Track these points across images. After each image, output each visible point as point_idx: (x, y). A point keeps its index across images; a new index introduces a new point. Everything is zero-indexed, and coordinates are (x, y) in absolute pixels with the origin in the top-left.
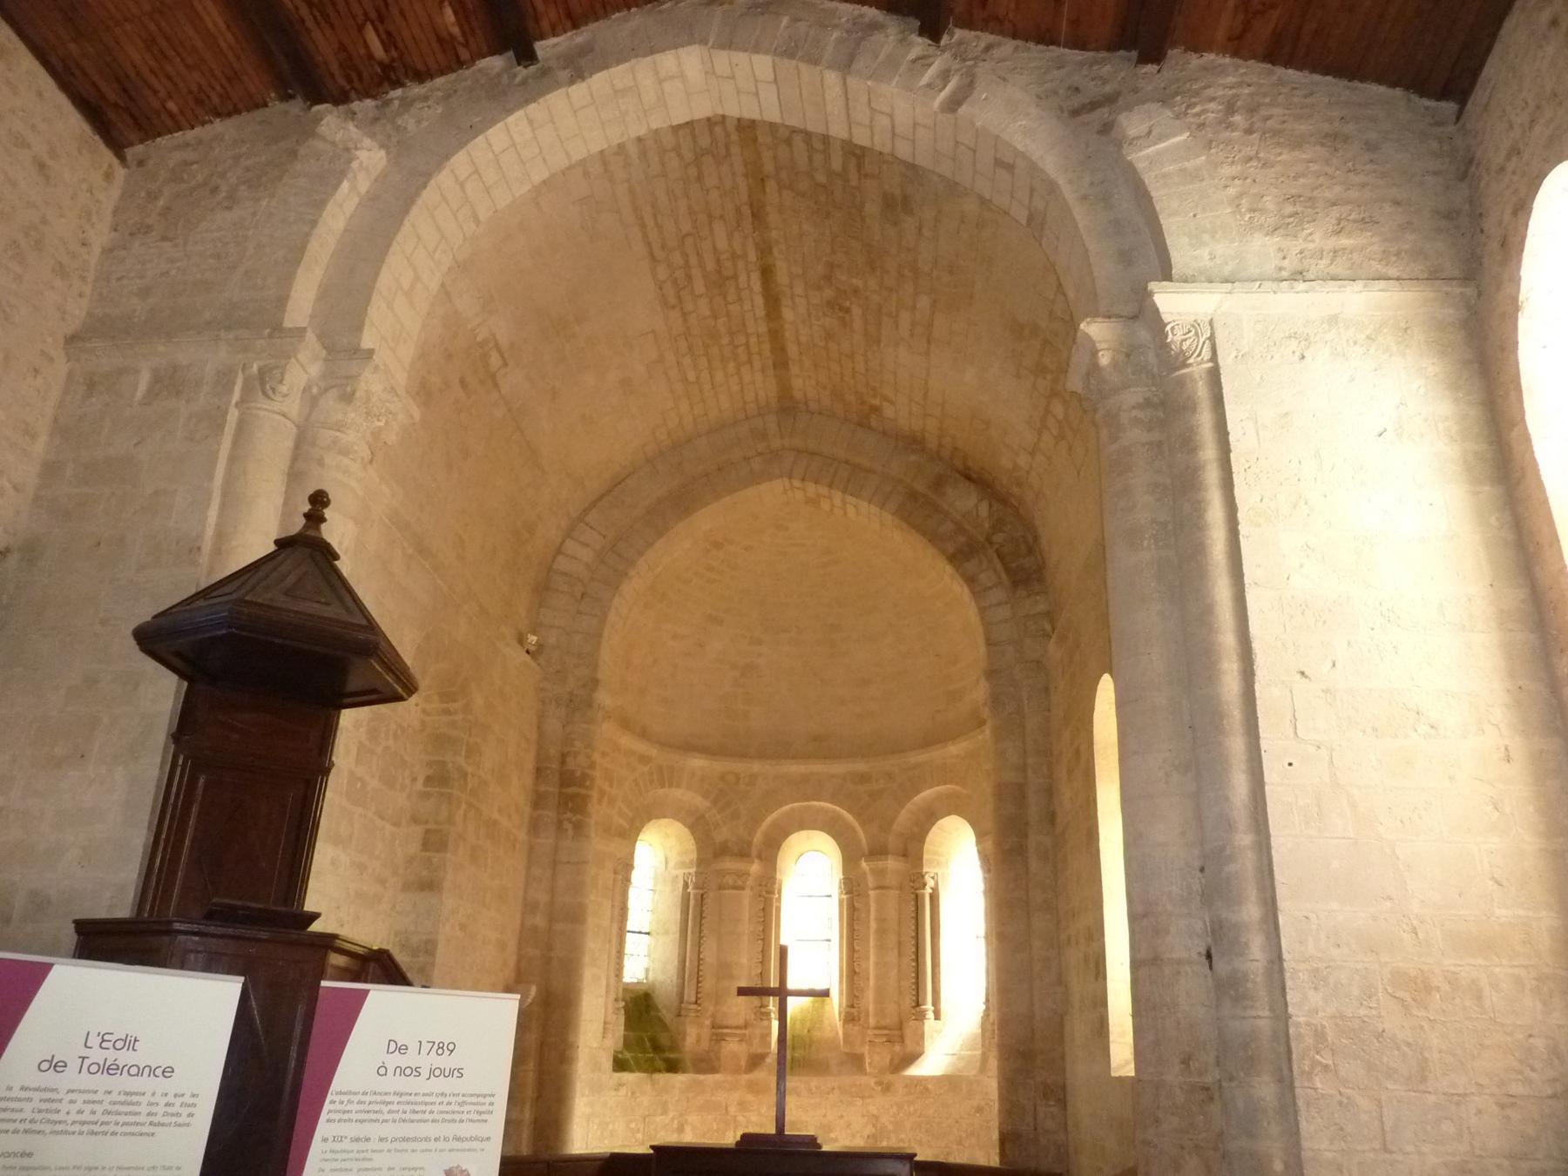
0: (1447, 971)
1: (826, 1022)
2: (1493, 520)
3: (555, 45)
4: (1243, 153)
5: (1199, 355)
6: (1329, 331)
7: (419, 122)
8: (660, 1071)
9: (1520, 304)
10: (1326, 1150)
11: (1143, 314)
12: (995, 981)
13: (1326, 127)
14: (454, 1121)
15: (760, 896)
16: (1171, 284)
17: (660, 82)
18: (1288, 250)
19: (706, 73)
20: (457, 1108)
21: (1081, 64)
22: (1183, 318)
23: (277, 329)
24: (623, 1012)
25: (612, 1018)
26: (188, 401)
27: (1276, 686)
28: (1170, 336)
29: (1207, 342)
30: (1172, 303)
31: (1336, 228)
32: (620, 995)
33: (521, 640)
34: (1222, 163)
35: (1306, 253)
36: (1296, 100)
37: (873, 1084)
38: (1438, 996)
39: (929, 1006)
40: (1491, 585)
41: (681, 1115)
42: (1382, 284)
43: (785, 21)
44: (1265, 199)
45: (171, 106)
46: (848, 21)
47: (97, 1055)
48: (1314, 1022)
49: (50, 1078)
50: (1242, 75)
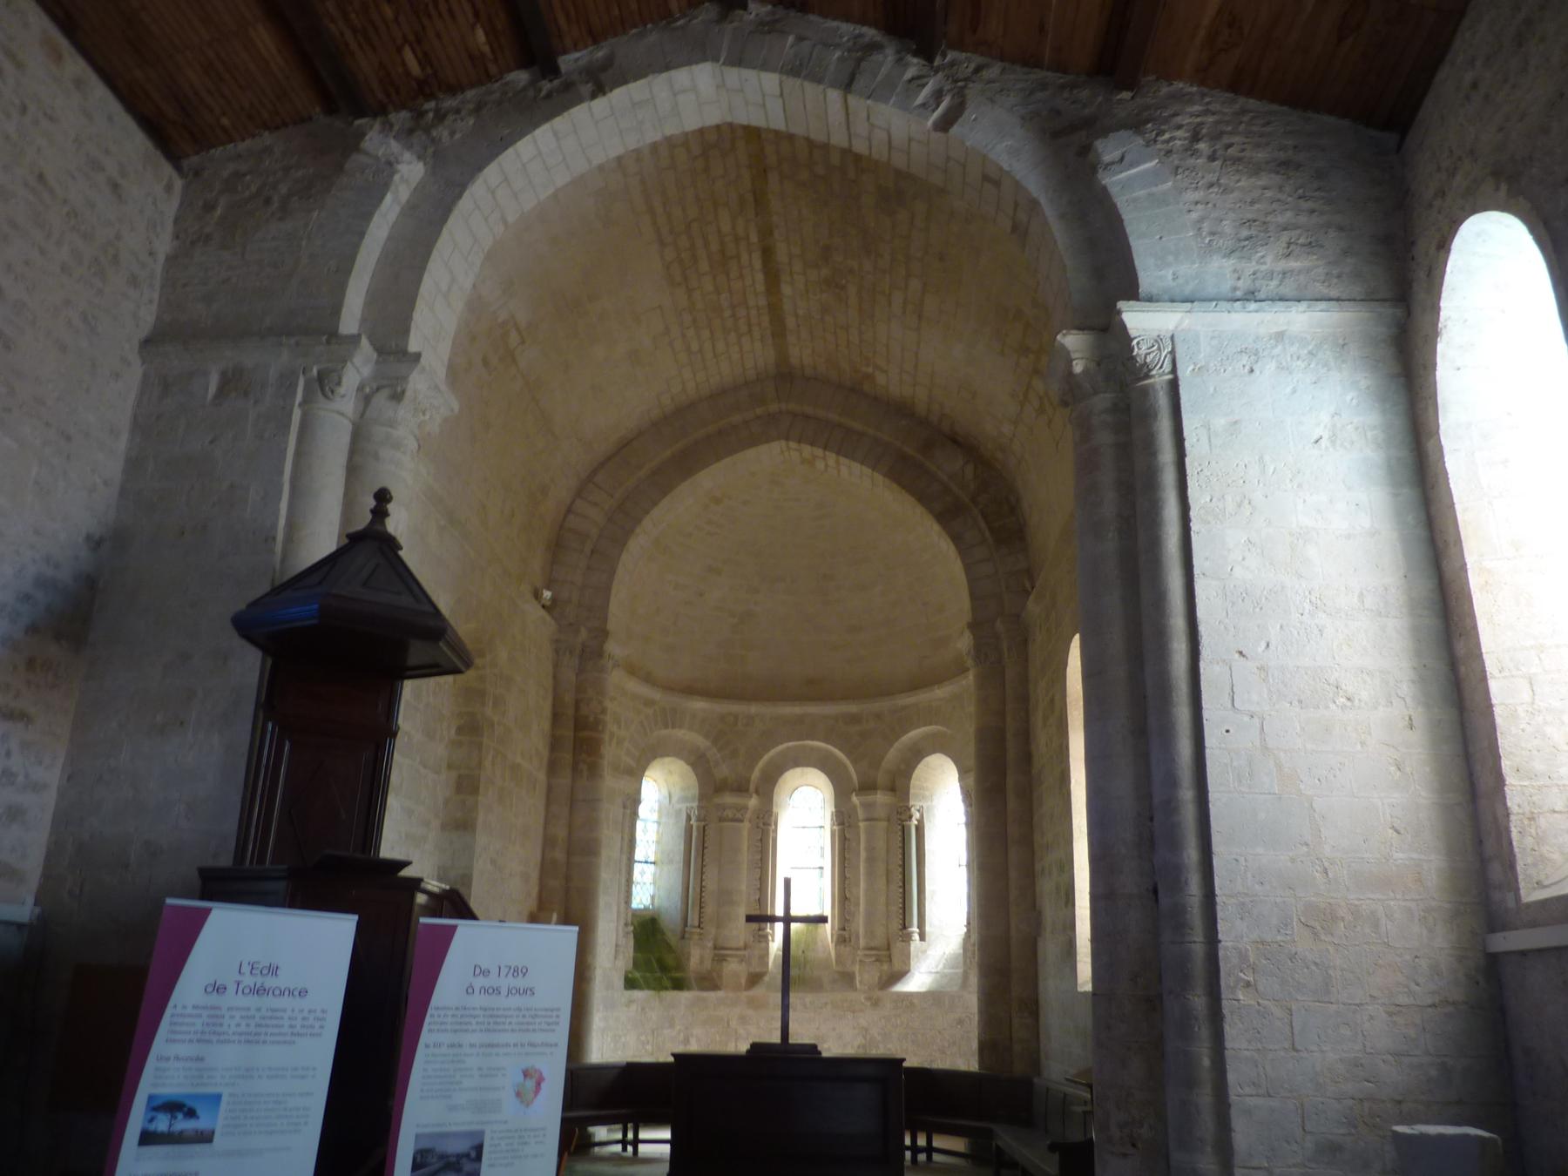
0: (1351, 904)
1: (820, 944)
2: (1410, 518)
3: (577, 60)
4: (1205, 180)
5: (1161, 367)
6: (1276, 346)
7: (452, 133)
8: (666, 989)
9: (1439, 330)
10: (1245, 1050)
11: (1110, 333)
12: (976, 906)
13: (1282, 155)
14: (528, 1030)
15: (758, 827)
16: (1138, 303)
17: (675, 95)
18: (1242, 271)
19: (718, 87)
20: (531, 1020)
21: (1063, 87)
22: (1147, 334)
23: (333, 335)
24: (632, 935)
25: (622, 941)
26: (256, 402)
27: (1218, 663)
28: (1136, 350)
29: (1168, 356)
30: (1140, 321)
31: (1285, 251)
32: (630, 921)
33: (537, 595)
34: (1186, 189)
35: (1258, 274)
36: (1255, 129)
37: (863, 1001)
38: (1342, 924)
39: (915, 929)
40: (1405, 576)
41: (687, 1028)
42: (1323, 305)
43: (791, 39)
44: (1224, 223)
45: (225, 121)
46: (848, 40)
47: (248, 980)
48: (1240, 946)
49: (214, 999)
50: (1208, 103)
